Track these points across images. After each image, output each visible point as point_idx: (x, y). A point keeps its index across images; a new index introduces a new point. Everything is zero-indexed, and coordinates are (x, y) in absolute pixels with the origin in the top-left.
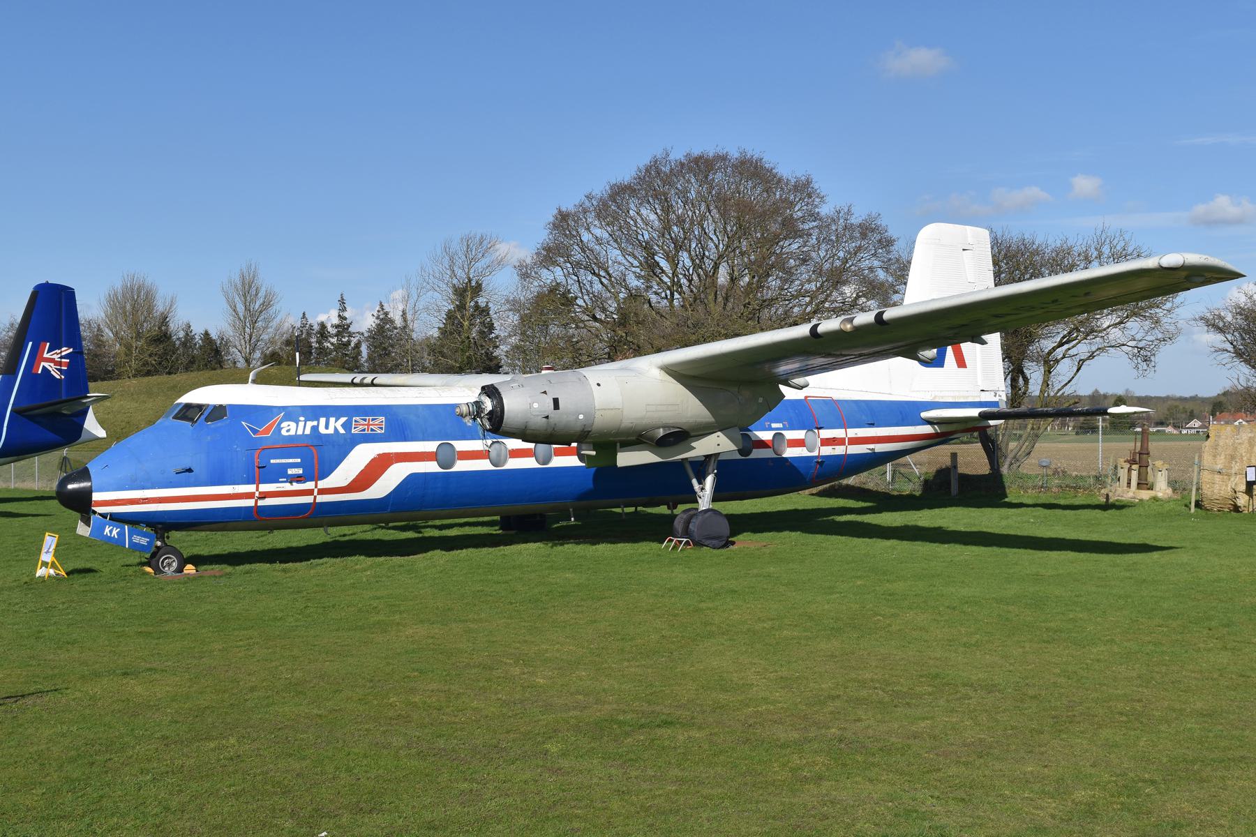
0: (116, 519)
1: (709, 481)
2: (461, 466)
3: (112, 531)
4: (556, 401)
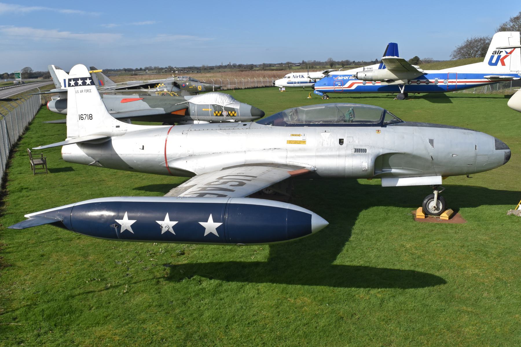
0: (317, 91)
1: (403, 88)
2: (367, 85)
3: (317, 92)
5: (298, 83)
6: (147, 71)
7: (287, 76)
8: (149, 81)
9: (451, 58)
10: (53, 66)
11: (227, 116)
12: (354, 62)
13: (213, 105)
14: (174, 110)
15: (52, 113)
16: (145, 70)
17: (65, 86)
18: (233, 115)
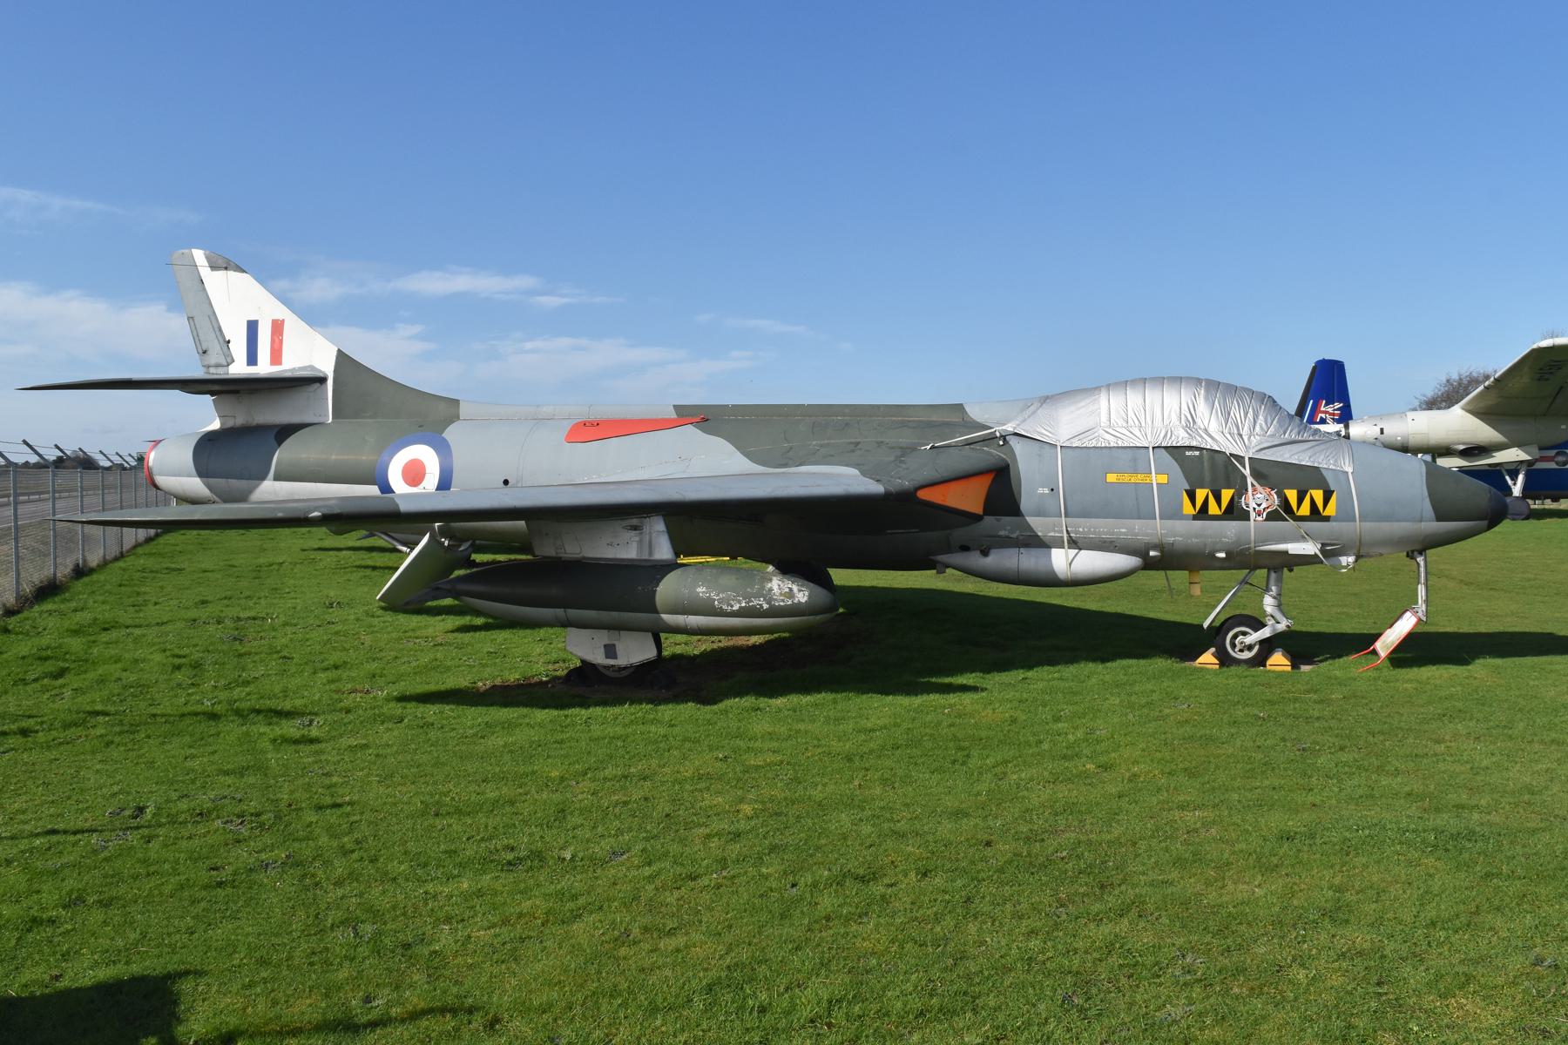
1: (1521, 478)
4: (1382, 431)
10: (199, 256)
11: (1273, 516)
13: (1176, 451)
14: (927, 474)
17: (252, 359)
18: (1315, 513)
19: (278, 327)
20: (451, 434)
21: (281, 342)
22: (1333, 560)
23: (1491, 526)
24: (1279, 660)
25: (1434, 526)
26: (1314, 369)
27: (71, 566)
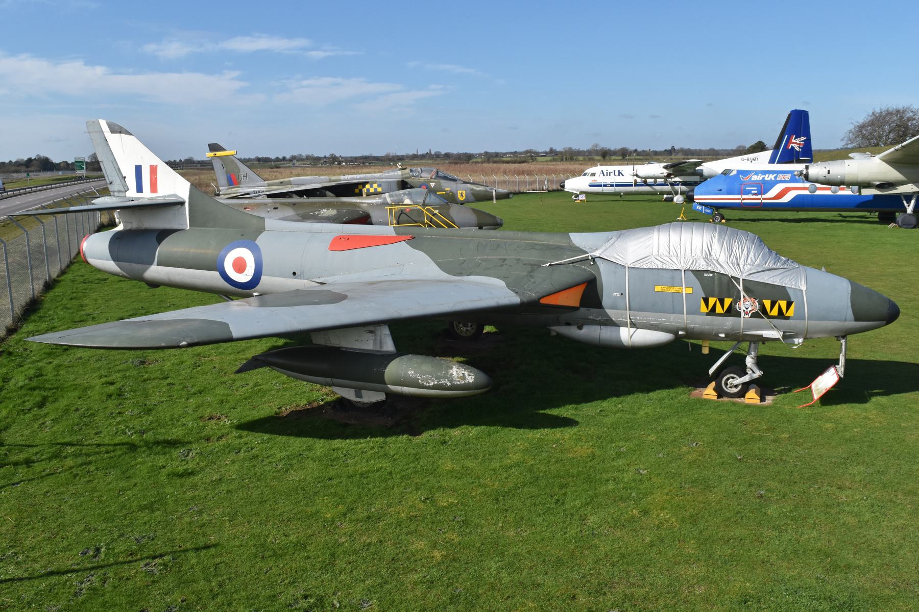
1: (913, 202)
2: (818, 193)
4: (829, 172)
5: (612, 186)
6: (295, 161)
7: (590, 171)
8: (342, 177)
9: (843, 143)
11: (755, 315)
12: (636, 150)
13: (698, 273)
14: (546, 287)
15: (102, 276)
16: (291, 160)
17: (140, 189)
19: (153, 170)
20: (261, 241)
21: (156, 179)
22: (789, 341)
23: (887, 324)
24: (752, 396)
25: (852, 324)
26: (790, 115)
27: (41, 282)
